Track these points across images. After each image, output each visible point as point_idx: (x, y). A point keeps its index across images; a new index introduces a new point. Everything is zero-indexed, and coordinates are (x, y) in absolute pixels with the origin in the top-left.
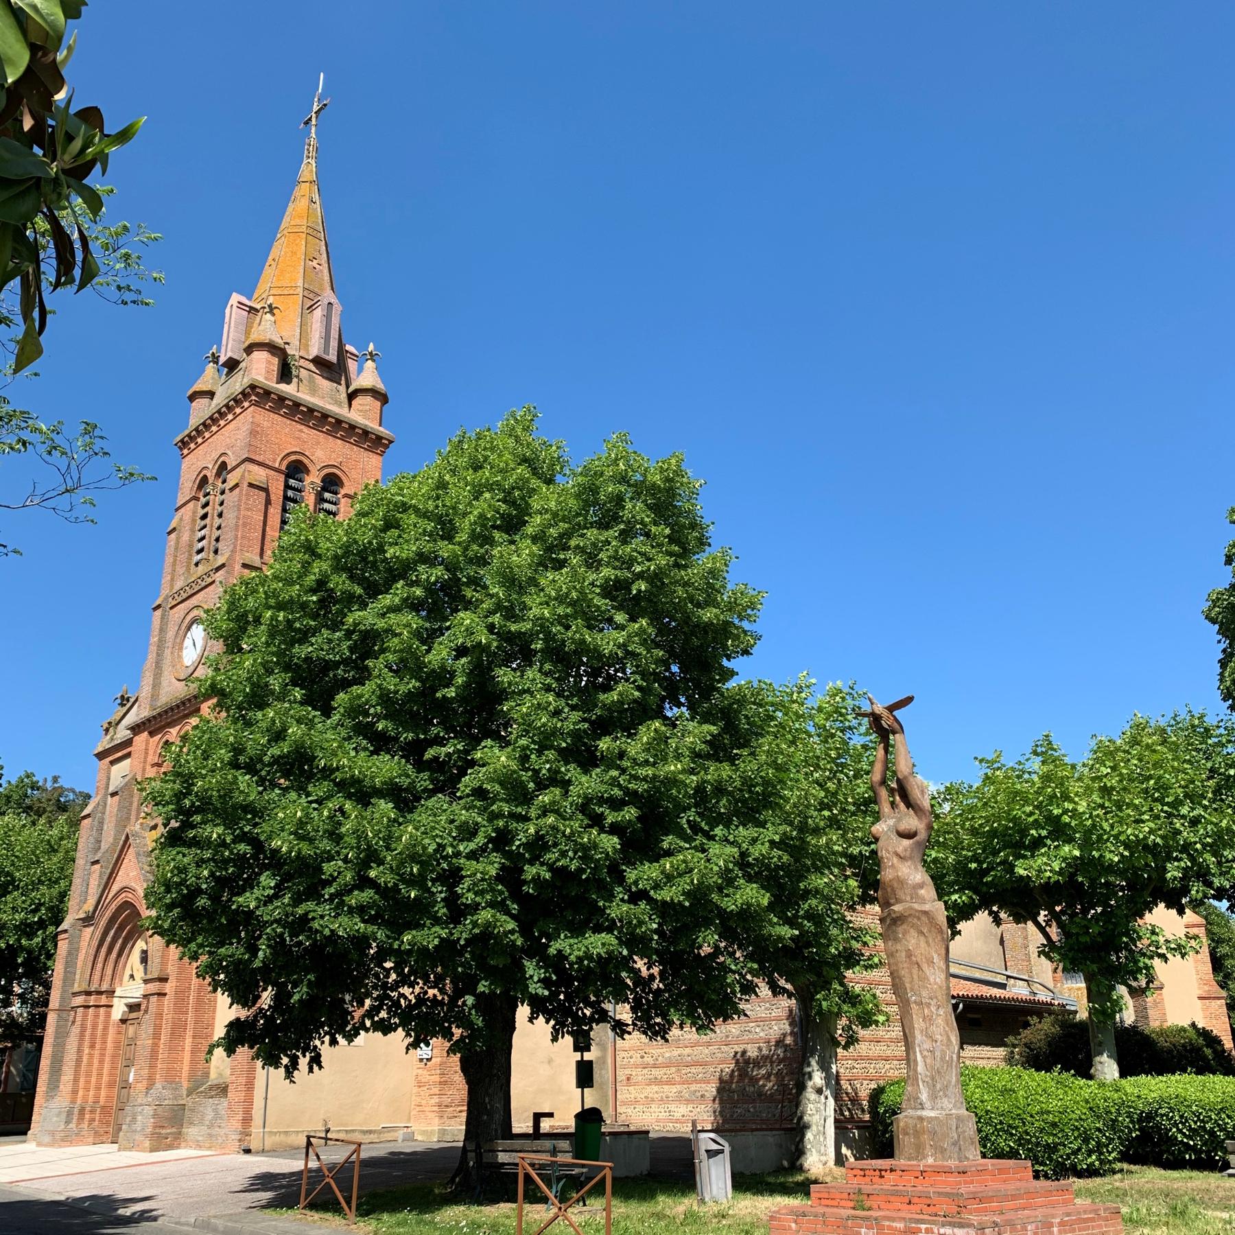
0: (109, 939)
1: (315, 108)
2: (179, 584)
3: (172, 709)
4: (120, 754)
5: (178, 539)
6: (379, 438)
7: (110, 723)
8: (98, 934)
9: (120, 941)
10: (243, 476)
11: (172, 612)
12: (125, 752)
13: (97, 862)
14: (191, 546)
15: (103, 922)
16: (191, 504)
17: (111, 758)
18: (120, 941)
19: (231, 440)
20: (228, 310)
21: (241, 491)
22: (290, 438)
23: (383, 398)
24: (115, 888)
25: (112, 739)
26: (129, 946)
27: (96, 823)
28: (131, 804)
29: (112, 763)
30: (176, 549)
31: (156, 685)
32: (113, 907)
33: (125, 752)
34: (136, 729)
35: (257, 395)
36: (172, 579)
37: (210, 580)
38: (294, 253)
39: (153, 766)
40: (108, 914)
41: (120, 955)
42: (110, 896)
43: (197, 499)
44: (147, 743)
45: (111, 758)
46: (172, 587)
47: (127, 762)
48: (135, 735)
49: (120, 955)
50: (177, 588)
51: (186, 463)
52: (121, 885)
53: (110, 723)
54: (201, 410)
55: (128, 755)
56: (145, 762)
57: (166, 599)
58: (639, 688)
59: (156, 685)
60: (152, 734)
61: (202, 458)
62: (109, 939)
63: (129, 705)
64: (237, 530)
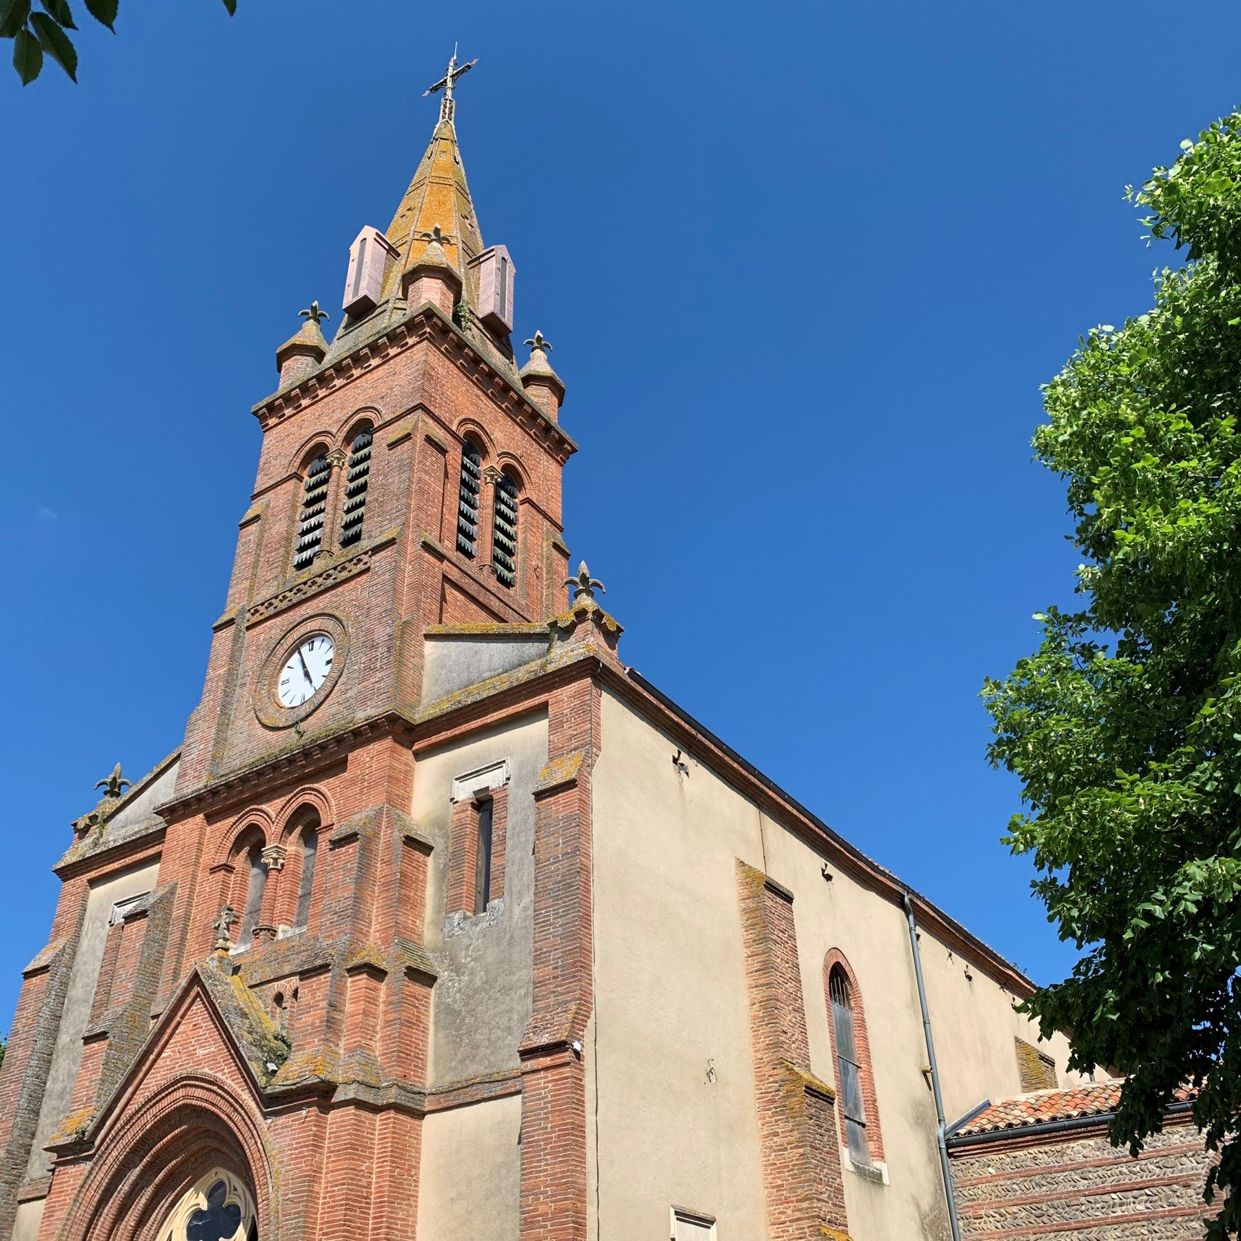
0: (124, 1187)
1: (451, 71)
2: (265, 593)
3: (275, 767)
4: (116, 865)
5: (262, 532)
6: (562, 441)
7: (93, 819)
8: (102, 1177)
9: (149, 1191)
10: (415, 426)
11: (249, 634)
12: (151, 852)
13: (102, 1036)
14: (288, 540)
15: (116, 1154)
16: (290, 485)
17: (93, 874)
18: (149, 1191)
19: (388, 385)
20: (355, 248)
21: (414, 444)
22: (464, 401)
23: (559, 391)
24: (153, 1083)
25: (96, 844)
26: (165, 1203)
27: (56, 984)
28: (165, 937)
29: (93, 883)
30: (259, 545)
31: (220, 740)
32: (149, 1120)
33: (151, 852)
34: (174, 812)
35: (433, 327)
36: (251, 587)
37: (361, 567)
38: (441, 203)
39: (213, 870)
40: (132, 1136)
41: (141, 1223)
42: (140, 1099)
43: (300, 479)
44: (202, 829)
45: (93, 874)
46: (250, 597)
47: (156, 868)
48: (170, 823)
49: (141, 1223)
50: (259, 599)
51: (269, 439)
52: (179, 1072)
53: (93, 819)
54: (299, 369)
55: (156, 858)
56: (197, 864)
57: (242, 612)
58: (1200, 757)
59: (220, 740)
60: (211, 819)
61: (327, 416)
62: (124, 1187)
63: (125, 797)
64: (409, 496)
